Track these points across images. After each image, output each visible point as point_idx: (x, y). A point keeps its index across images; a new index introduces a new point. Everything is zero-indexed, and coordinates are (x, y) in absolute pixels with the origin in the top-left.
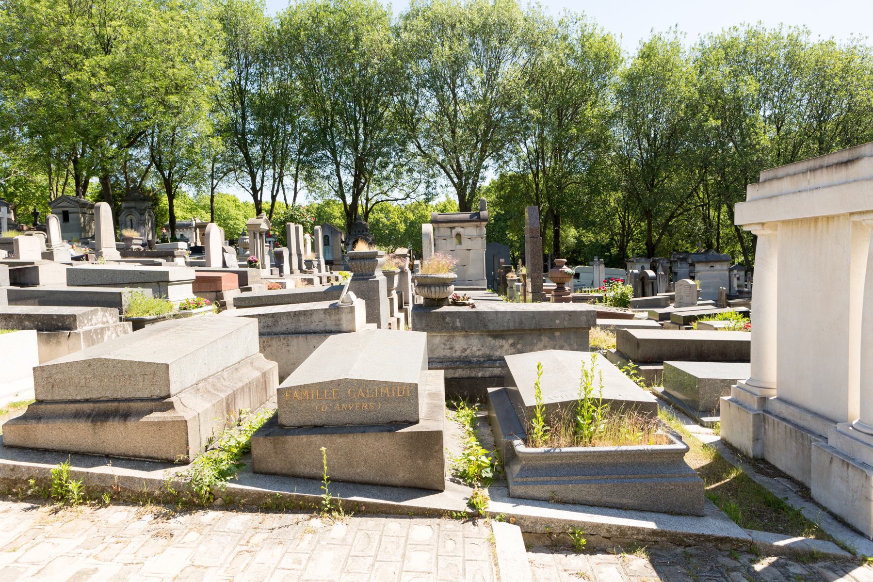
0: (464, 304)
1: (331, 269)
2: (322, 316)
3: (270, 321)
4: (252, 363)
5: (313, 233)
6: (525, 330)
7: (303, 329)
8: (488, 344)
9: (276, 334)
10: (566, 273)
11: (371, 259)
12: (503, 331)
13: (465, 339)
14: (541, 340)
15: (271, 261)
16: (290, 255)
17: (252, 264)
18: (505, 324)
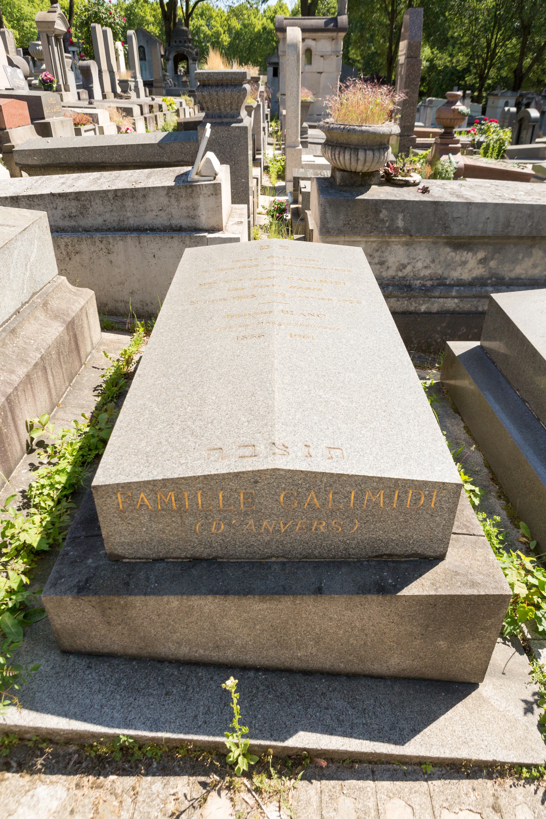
0: (407, 184)
1: (151, 93)
2: (164, 200)
3: (73, 207)
4: (45, 304)
5: (126, 41)
6: (509, 237)
7: (132, 222)
8: (442, 258)
9: (86, 230)
10: (459, 113)
11: (235, 86)
12: (474, 237)
13: (405, 248)
14: (530, 255)
15: (77, 78)
16: (100, 72)
17: (47, 85)
18: (480, 226)
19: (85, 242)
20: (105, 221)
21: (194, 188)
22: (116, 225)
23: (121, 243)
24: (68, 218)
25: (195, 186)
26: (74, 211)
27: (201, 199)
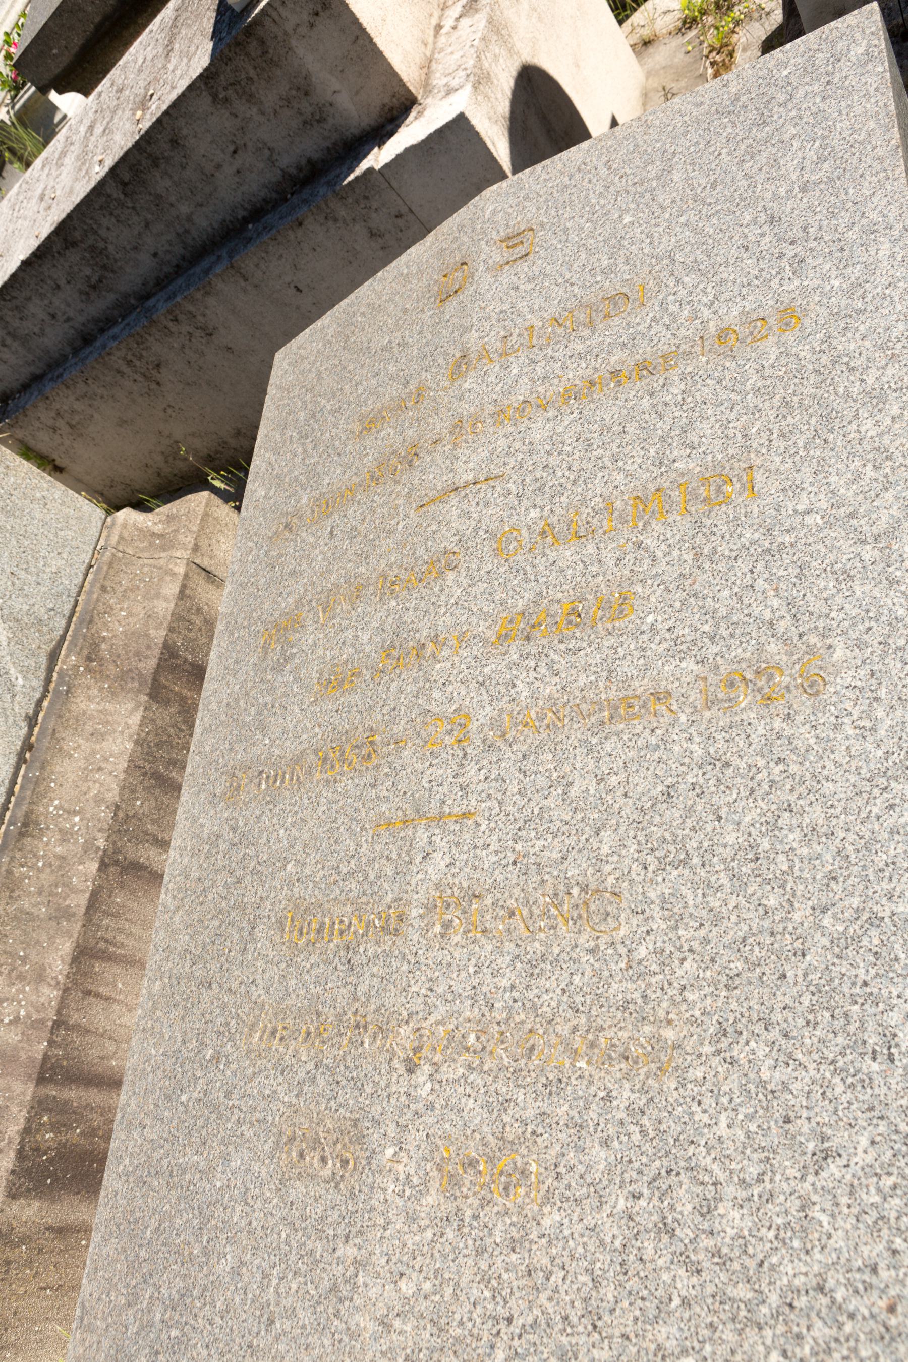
19: (151, 339)
20: (155, 255)
21: (260, 31)
22: (182, 251)
23: (211, 301)
24: (93, 295)
25: (257, 21)
26: (88, 271)
27: (300, 52)
